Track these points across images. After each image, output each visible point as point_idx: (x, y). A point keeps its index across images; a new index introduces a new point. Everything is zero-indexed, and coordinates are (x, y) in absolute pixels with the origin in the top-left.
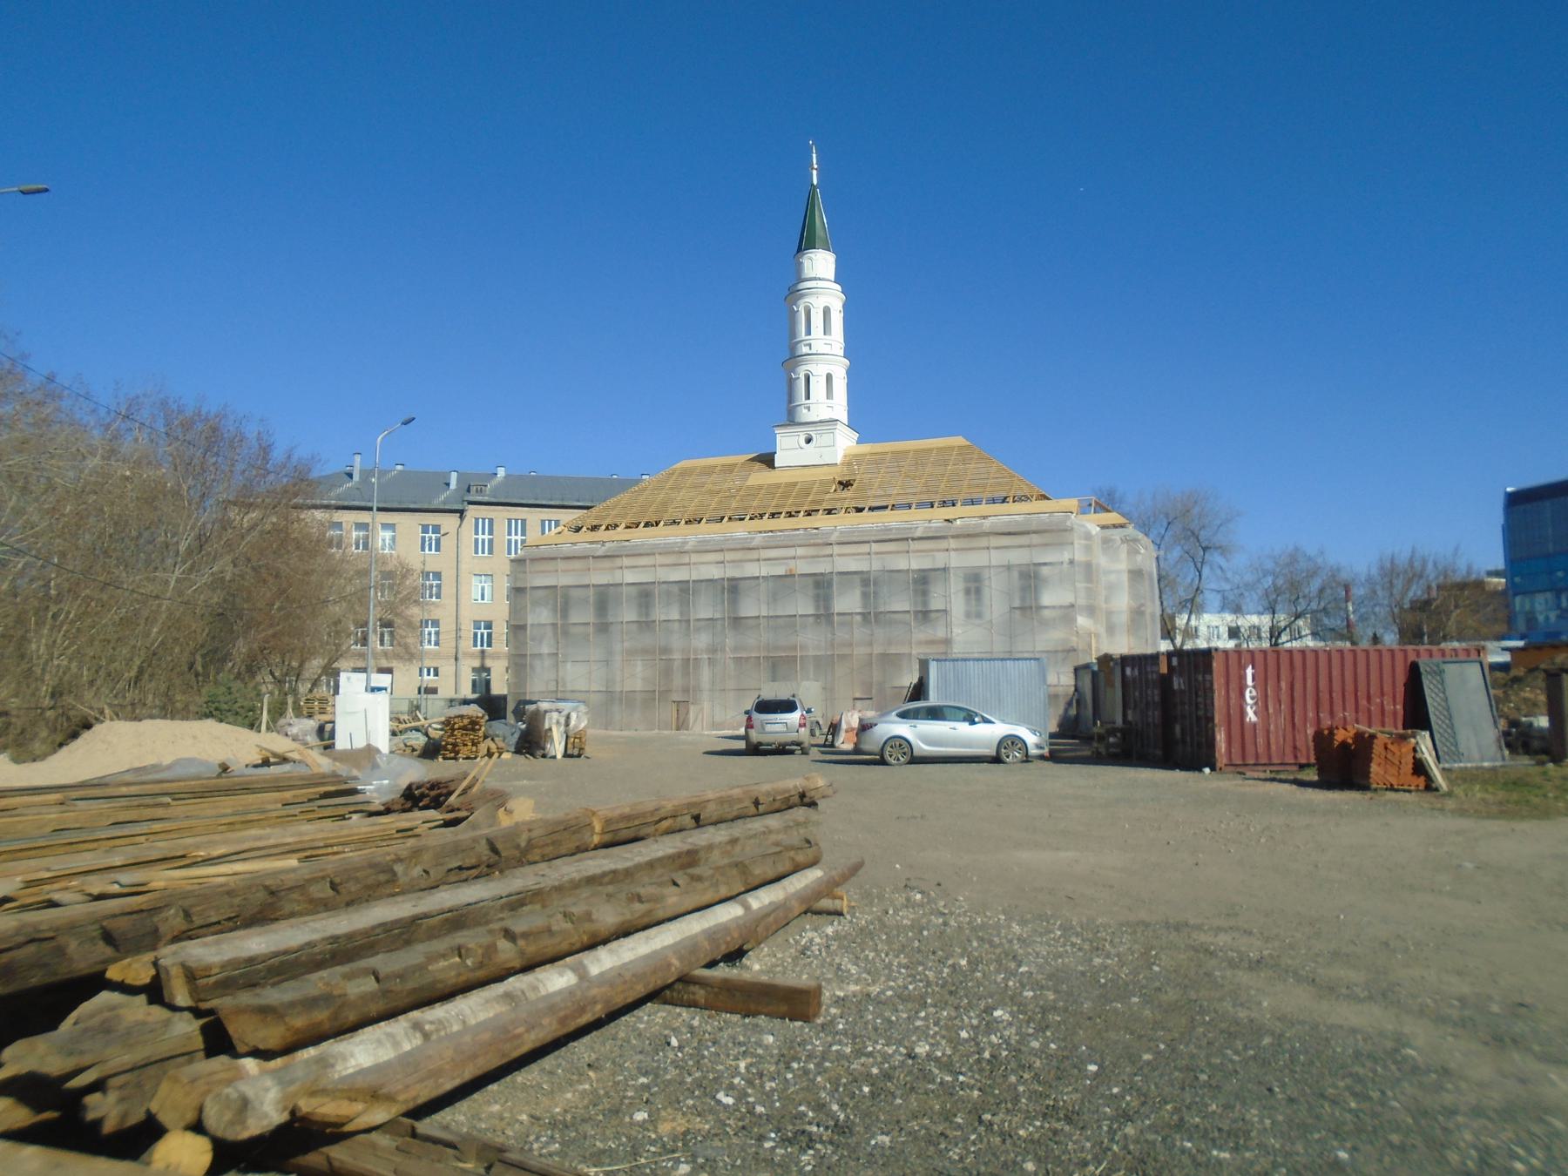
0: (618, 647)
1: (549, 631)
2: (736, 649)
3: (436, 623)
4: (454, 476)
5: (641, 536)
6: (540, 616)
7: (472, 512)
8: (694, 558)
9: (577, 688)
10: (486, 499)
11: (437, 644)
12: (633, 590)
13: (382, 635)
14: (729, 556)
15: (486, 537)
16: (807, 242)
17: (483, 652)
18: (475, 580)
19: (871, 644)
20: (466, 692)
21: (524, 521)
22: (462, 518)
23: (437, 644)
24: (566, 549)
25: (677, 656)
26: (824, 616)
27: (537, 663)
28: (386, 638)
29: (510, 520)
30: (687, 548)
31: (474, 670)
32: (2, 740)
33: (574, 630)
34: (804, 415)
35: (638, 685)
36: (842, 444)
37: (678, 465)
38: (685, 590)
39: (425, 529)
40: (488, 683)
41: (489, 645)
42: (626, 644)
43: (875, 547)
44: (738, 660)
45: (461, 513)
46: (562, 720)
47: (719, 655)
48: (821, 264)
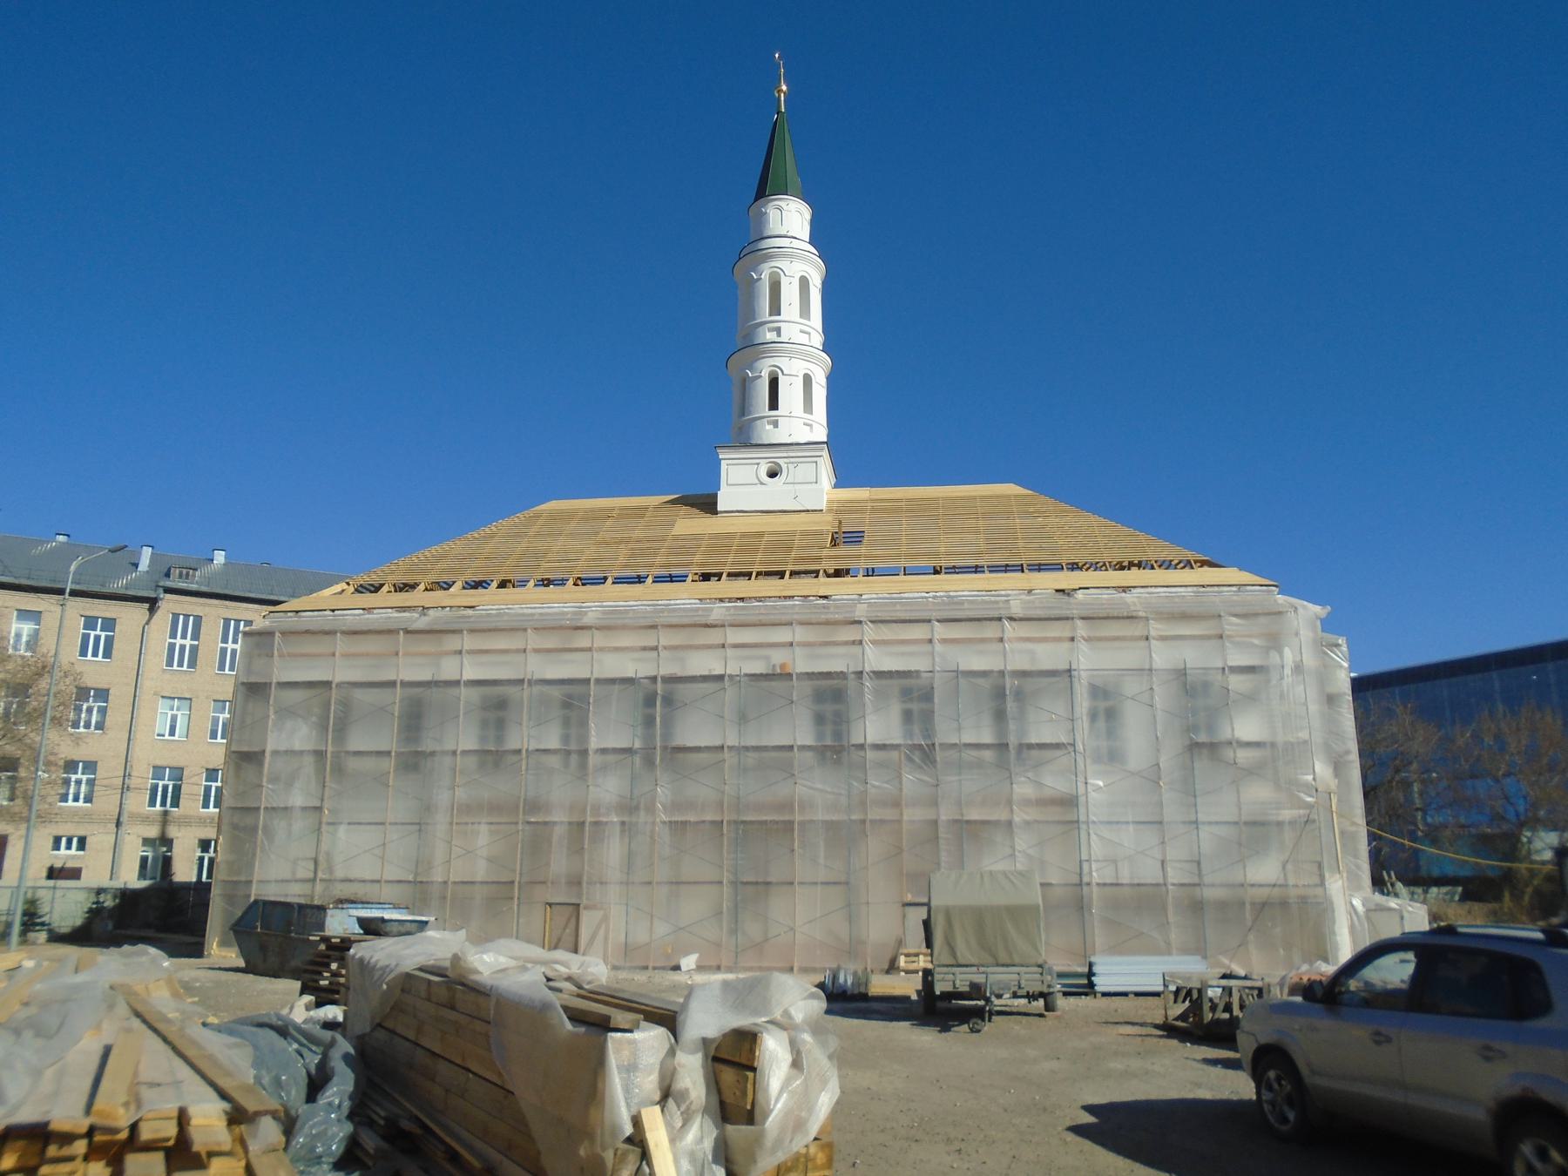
0: (443, 797)
1: (309, 762)
2: (675, 806)
3: (90, 766)
4: (147, 553)
5: (491, 601)
6: (290, 736)
7: (169, 604)
8: (600, 640)
9: (356, 873)
10: (194, 587)
11: (88, 799)
12: (473, 695)
14: (665, 639)
15: (188, 642)
16: (765, 189)
17: (166, 813)
18: (163, 706)
19: (935, 803)
20: (130, 878)
23: (88, 799)
24: (353, 618)
25: (559, 817)
26: (835, 750)
27: (279, 825)
29: (227, 621)
30: (587, 620)
31: (147, 842)
33: (353, 764)
34: (767, 433)
35: (481, 871)
36: (813, 488)
37: (543, 507)
38: (573, 700)
39: (90, 623)
40: (167, 862)
41: (176, 803)
42: (461, 794)
43: (940, 631)
44: (678, 828)
45: (152, 604)
46: (692, 1075)
47: (642, 817)
48: (790, 218)
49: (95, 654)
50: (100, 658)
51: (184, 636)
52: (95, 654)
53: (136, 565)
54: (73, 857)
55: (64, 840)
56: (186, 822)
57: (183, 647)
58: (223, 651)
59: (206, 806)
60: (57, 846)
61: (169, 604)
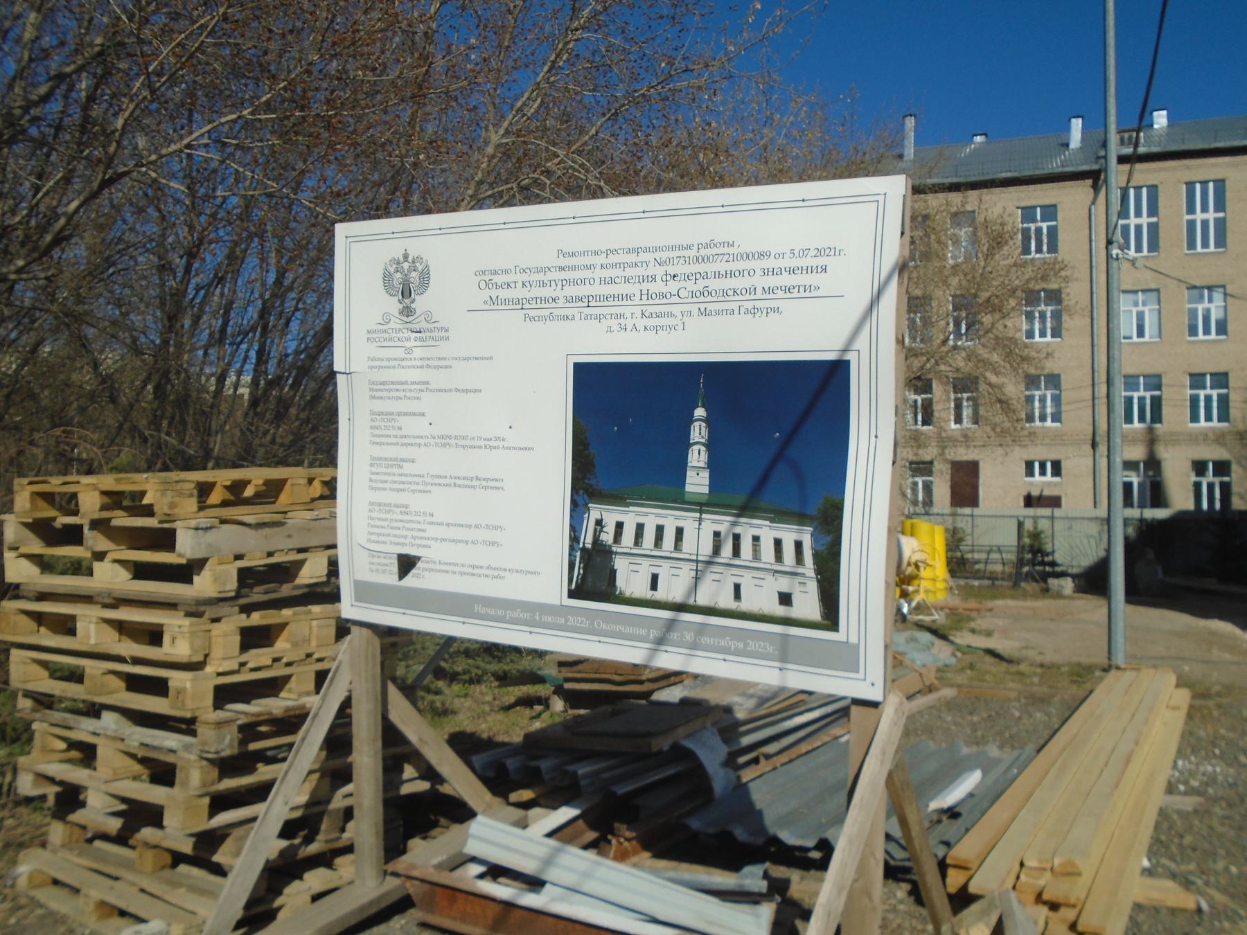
11: (1056, 417)
13: (958, 407)
15: (1211, 216)
21: (1220, 184)
22: (1095, 187)
28: (966, 413)
29: (1190, 185)
32: (306, 2)
50: (1212, 248)
51: (1205, 209)
54: (1049, 484)
55: (1037, 465)
56: (1176, 439)
57: (1205, 224)
58: (1191, 224)
59: (1194, 418)
60: (1030, 471)
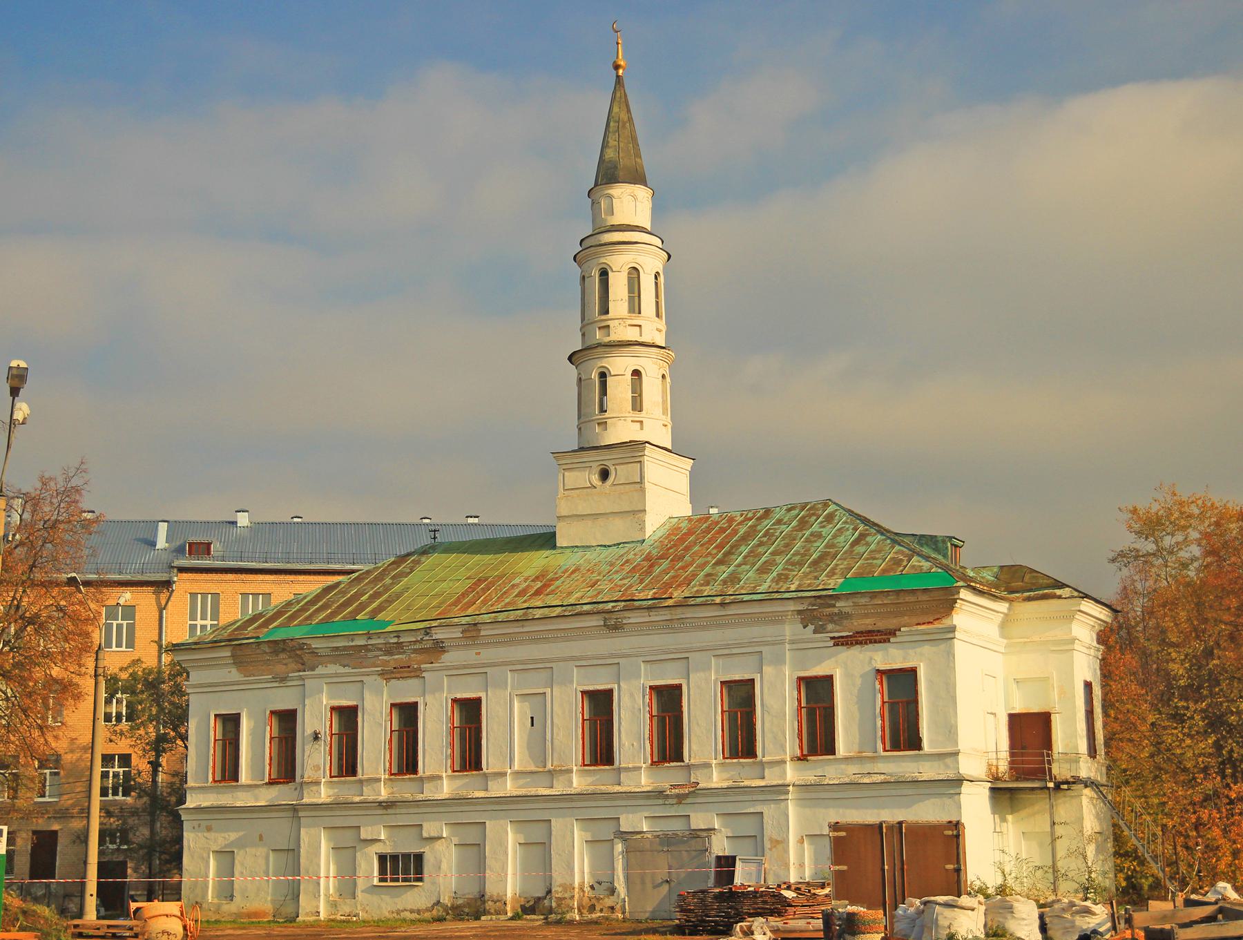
7: (184, 585)
15: (199, 622)
49: (119, 645)
52: (119, 645)
53: (153, 544)
61: (184, 585)
